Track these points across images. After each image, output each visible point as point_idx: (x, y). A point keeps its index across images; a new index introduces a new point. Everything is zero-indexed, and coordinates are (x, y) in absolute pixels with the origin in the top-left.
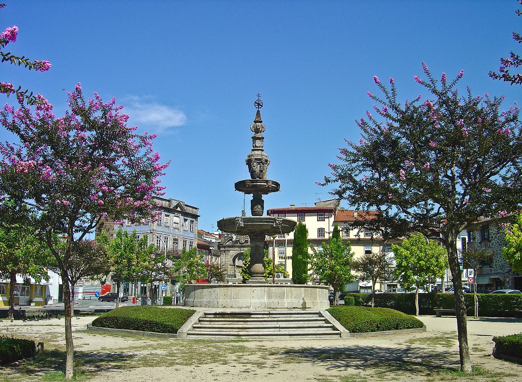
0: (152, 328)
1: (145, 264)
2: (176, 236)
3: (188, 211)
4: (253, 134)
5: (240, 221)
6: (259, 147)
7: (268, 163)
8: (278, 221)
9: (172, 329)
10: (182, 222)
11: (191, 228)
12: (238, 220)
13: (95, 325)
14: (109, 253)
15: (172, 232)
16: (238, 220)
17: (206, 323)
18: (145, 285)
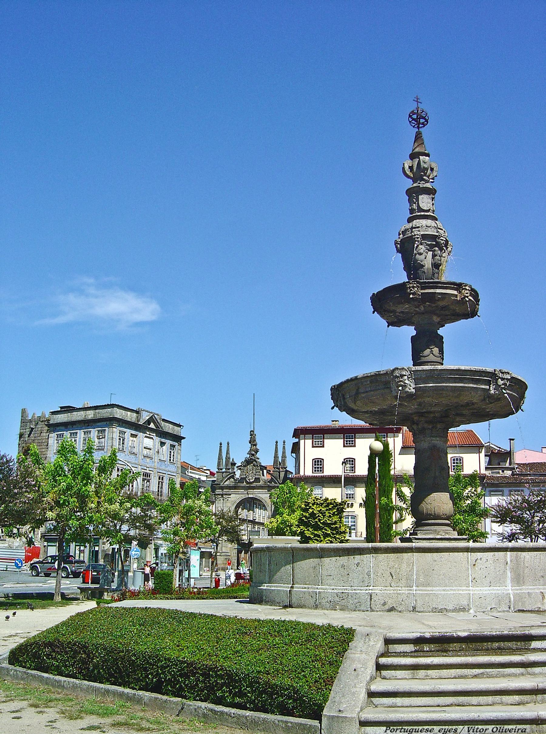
0: (211, 689)
1: (113, 507)
2: (148, 469)
3: (166, 430)
4: (409, 184)
5: (406, 377)
6: (428, 211)
7: (449, 249)
8: (503, 379)
9: (295, 700)
10: (157, 447)
11: (170, 457)
12: (402, 376)
13: (18, 661)
14: (45, 486)
15: (141, 462)
16: (402, 376)
17: (400, 673)
18: (97, 548)
